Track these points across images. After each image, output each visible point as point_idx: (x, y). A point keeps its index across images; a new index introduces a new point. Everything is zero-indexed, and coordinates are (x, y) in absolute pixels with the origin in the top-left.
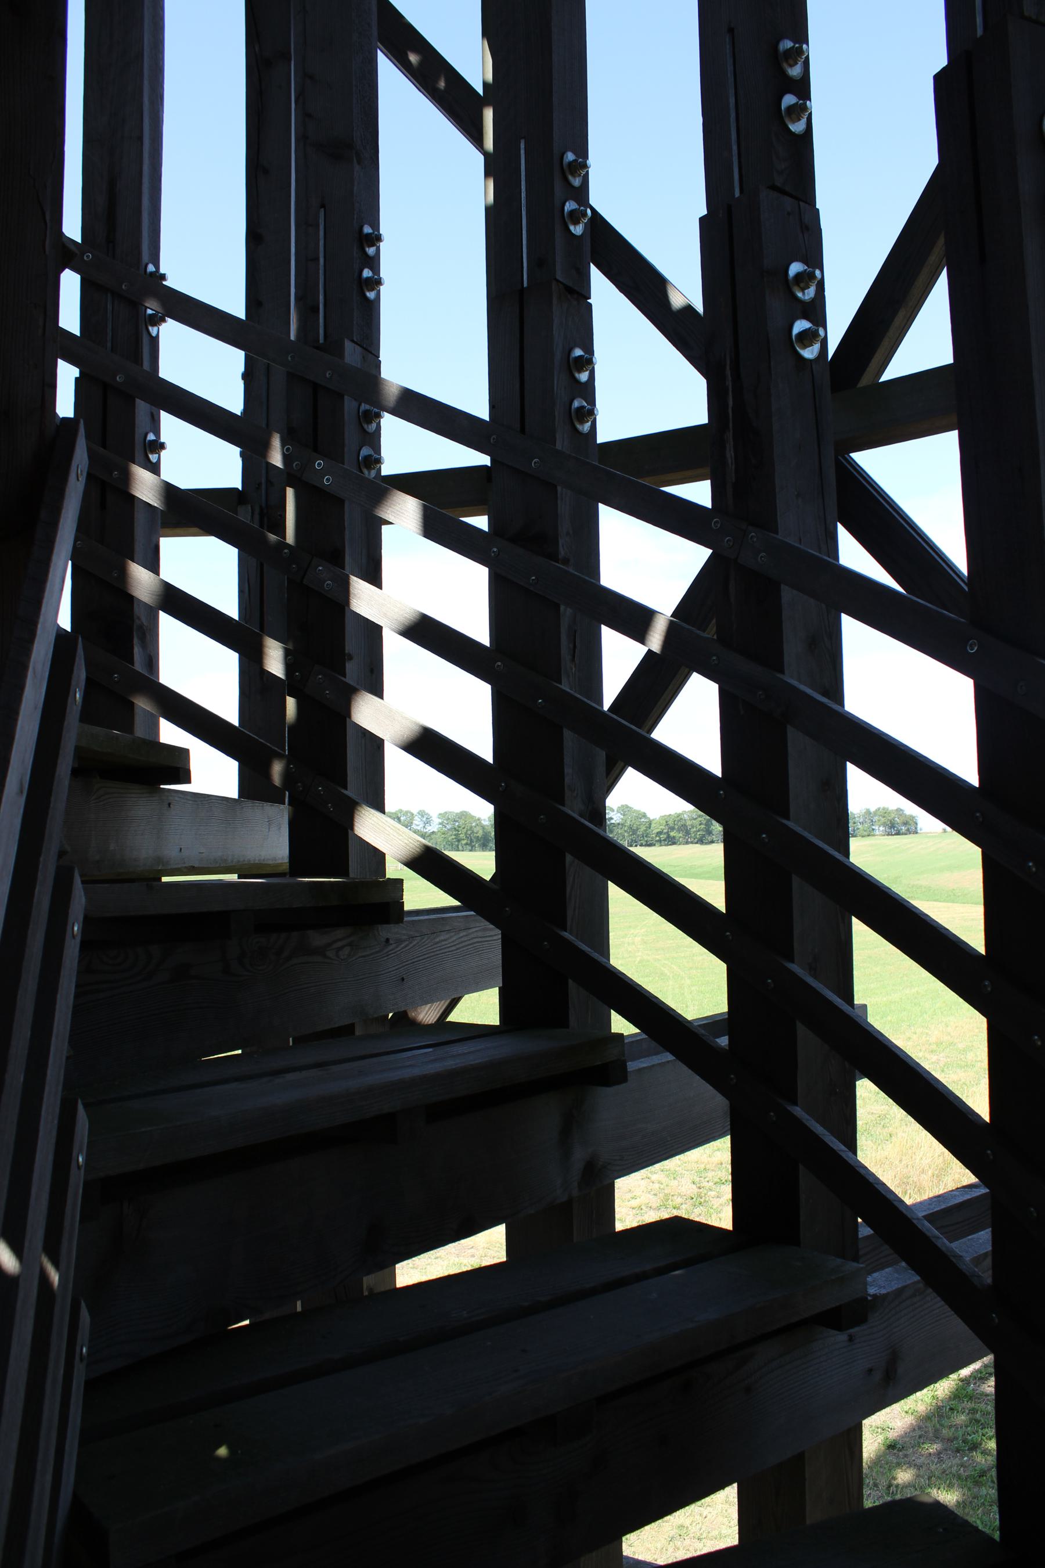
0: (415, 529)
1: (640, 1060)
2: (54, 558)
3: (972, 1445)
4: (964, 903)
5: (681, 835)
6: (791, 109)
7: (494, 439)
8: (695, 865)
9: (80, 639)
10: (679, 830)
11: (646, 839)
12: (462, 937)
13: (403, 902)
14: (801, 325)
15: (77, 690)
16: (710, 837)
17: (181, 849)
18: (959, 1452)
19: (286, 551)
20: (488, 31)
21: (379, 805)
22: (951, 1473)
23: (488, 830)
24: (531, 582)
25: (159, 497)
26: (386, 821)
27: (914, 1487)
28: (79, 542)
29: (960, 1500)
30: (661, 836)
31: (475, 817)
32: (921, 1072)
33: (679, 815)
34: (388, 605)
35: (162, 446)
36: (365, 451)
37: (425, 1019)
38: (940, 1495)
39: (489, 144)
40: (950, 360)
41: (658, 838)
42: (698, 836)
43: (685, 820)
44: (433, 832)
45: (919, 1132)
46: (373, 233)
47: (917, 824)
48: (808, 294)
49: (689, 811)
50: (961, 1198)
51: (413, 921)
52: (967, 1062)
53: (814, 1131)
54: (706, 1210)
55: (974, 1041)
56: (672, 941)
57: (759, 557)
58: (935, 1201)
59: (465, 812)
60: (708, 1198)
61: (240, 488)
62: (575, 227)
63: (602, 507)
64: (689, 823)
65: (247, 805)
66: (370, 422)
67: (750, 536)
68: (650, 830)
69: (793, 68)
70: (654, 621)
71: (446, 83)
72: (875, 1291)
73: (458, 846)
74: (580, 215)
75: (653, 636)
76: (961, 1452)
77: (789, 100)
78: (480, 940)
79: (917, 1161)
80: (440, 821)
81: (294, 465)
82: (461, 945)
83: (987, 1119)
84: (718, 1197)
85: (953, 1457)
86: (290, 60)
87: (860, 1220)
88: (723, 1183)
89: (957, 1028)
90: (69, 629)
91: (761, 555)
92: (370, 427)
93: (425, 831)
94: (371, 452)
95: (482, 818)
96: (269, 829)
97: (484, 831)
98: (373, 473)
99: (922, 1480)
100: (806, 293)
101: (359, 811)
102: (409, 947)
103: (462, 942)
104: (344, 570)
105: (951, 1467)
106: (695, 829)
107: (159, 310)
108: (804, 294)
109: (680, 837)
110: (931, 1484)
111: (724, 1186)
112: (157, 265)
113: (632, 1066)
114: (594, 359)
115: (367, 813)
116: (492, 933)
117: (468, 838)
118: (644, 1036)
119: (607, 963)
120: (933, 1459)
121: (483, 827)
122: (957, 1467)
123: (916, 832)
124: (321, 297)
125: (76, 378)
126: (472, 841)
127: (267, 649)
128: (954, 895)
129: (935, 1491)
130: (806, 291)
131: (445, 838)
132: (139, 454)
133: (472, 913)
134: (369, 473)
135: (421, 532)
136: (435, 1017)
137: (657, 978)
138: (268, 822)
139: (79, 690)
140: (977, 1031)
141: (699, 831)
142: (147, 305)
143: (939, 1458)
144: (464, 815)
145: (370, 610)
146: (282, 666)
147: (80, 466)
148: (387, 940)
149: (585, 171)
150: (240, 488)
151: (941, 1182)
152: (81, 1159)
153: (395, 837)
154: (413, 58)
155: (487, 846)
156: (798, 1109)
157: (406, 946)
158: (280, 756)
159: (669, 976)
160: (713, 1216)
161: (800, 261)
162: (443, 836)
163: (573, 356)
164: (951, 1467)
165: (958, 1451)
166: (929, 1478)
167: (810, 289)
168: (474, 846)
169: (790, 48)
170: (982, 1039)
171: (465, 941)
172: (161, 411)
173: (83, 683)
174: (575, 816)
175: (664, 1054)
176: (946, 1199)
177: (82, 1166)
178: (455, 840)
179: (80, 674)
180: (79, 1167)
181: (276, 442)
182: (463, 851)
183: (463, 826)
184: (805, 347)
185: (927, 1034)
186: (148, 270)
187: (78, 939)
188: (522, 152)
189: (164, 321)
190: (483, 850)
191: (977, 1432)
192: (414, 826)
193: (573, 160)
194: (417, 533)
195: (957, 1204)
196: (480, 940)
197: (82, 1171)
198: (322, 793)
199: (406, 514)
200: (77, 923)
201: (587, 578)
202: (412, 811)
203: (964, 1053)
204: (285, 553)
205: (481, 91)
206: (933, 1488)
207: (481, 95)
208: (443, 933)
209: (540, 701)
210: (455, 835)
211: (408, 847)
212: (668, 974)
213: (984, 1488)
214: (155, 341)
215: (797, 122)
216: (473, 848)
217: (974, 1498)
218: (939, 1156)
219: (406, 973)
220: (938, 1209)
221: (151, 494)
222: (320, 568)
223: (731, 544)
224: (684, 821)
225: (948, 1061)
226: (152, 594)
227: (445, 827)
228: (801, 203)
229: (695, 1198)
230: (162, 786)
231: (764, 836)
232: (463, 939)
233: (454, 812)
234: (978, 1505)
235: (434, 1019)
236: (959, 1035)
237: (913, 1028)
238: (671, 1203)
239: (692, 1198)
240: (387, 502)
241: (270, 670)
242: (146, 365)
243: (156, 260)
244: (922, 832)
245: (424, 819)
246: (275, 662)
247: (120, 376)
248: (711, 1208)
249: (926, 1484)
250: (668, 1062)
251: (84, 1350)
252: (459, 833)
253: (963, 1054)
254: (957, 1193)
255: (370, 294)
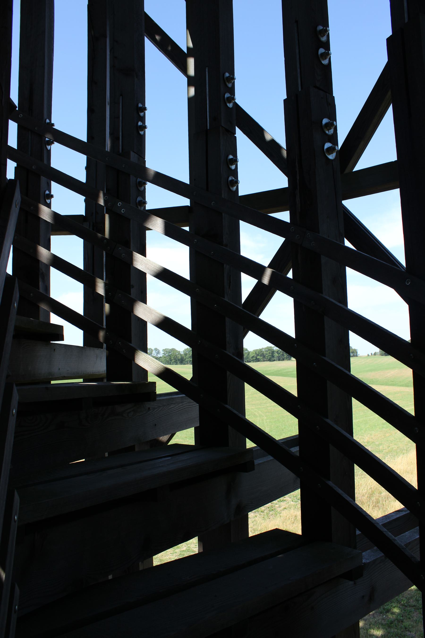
0: (161, 232)
1: (259, 459)
2: (5, 242)
3: (387, 610)
4: (377, 385)
5: (261, 358)
6: (322, 54)
7: (195, 193)
8: (267, 370)
9: (17, 279)
10: (261, 356)
11: (247, 359)
12: (180, 406)
13: (156, 392)
14: (328, 145)
15: (15, 302)
16: (273, 359)
17: (59, 369)
18: (381, 614)
19: (105, 241)
20: (189, 26)
21: (145, 350)
22: (378, 622)
23: (183, 356)
24: (211, 254)
25: (50, 218)
26: (149, 357)
27: (364, 629)
28: (16, 237)
29: (383, 634)
30: (254, 358)
31: (178, 351)
32: (386, 467)
33: (261, 350)
34: (149, 264)
35: (52, 196)
36: (139, 199)
37: (162, 439)
38: (375, 632)
39: (191, 71)
40: (396, 159)
41: (252, 359)
42: (268, 358)
43: (263, 352)
44: (161, 357)
45: (361, 479)
46: (143, 107)
47: (357, 353)
48: (331, 132)
49: (265, 348)
50: (396, 516)
51: (160, 400)
52: (380, 450)
53: (338, 492)
54: (275, 513)
55: (382, 441)
56: (258, 401)
57: (312, 244)
58: (385, 518)
59: (174, 349)
60: (275, 508)
61: (84, 215)
62: (229, 104)
63: (241, 222)
64: (265, 353)
65: (87, 349)
66: (141, 186)
67: (307, 235)
68: (249, 356)
69: (323, 37)
70: (265, 271)
71: (171, 48)
72: (364, 561)
73: (170, 363)
74: (232, 99)
75: (265, 278)
76: (382, 613)
77: (322, 51)
78: (188, 407)
79: (361, 491)
80: (163, 352)
81: (109, 204)
82: (180, 410)
83: (417, 488)
84: (279, 507)
85: (379, 615)
86: (106, 37)
87: (358, 532)
88: (281, 501)
89: (375, 436)
90: (11, 274)
91: (312, 243)
92: (141, 188)
93: (157, 356)
94: (142, 199)
95: (181, 351)
96: (97, 359)
97: (181, 357)
98: (142, 208)
99: (367, 626)
100: (330, 132)
101: (137, 353)
102: (158, 411)
103: (180, 408)
104: (130, 249)
105: (379, 620)
106: (267, 355)
107: (51, 138)
108: (329, 132)
109: (261, 359)
110: (371, 627)
111: (282, 502)
112: (50, 119)
113: (256, 462)
114: (238, 160)
115: (140, 354)
116: (193, 404)
117: (175, 359)
118: (259, 448)
119: (244, 418)
120: (371, 617)
121: (181, 355)
122: (381, 620)
123: (357, 356)
124: (121, 133)
125: (15, 167)
126: (176, 361)
127: (97, 283)
128: (373, 381)
129: (372, 630)
130: (330, 131)
131: (165, 359)
132: (42, 200)
133: (184, 395)
134: (141, 208)
135: (163, 233)
136: (167, 438)
137: (253, 416)
138: (96, 356)
139: (16, 302)
140: (383, 437)
141: (269, 356)
142: (46, 136)
143: (373, 616)
144: (173, 350)
145: (141, 266)
146: (103, 290)
147: (17, 201)
148: (149, 408)
149: (234, 80)
150: (84, 215)
151: (371, 500)
152: (16, 518)
153: (153, 364)
154: (158, 38)
155: (182, 362)
156: (330, 482)
157: (157, 410)
158: (103, 329)
159: (258, 415)
160: (277, 515)
161: (327, 118)
162: (164, 358)
163: (229, 158)
164: (379, 620)
165: (381, 613)
166: (370, 625)
167: (331, 130)
168: (177, 363)
169: (322, 29)
170: (385, 440)
171: (181, 408)
172: (52, 181)
173: (18, 299)
174: (231, 355)
175: (268, 456)
176: (389, 517)
177: (16, 521)
178: (169, 360)
179: (17, 295)
180: (15, 521)
181: (101, 195)
182: (173, 364)
183: (173, 355)
184: (329, 154)
185: (363, 438)
186: (46, 122)
187: (15, 416)
188: (207, 72)
189: (53, 143)
190: (181, 364)
191: (389, 605)
192: (153, 355)
193: (228, 76)
194: (162, 234)
195: (394, 519)
196: (188, 407)
197: (17, 522)
198: (121, 345)
199: (157, 225)
200: (15, 409)
201: (235, 253)
202: (152, 348)
203: (379, 446)
204: (105, 242)
205: (186, 51)
206: (371, 629)
207: (186, 53)
208: (172, 404)
209: (216, 305)
210: (169, 358)
211: (158, 368)
212: (257, 415)
213: (392, 629)
214: (49, 152)
215: (325, 60)
216: (177, 363)
217: (389, 633)
218: (370, 489)
219: (157, 422)
220: (387, 522)
221: (47, 217)
222: (120, 248)
223: (299, 238)
224: (263, 352)
225: (372, 450)
226: (47, 259)
227: (165, 355)
228: (327, 94)
229: (270, 508)
230: (51, 342)
231: (315, 364)
232: (180, 407)
233: (169, 349)
234: (390, 636)
235: (166, 439)
236: (376, 439)
237: (357, 436)
238: (260, 510)
239: (269, 508)
240: (149, 220)
241: (98, 292)
242: (45, 162)
243: (50, 118)
244: (359, 356)
245: (157, 352)
246: (101, 290)
247: (34, 166)
248: (277, 512)
249: (368, 627)
250: (270, 460)
251: (17, 607)
252: (171, 357)
253: (378, 447)
254: (394, 514)
255: (141, 132)
